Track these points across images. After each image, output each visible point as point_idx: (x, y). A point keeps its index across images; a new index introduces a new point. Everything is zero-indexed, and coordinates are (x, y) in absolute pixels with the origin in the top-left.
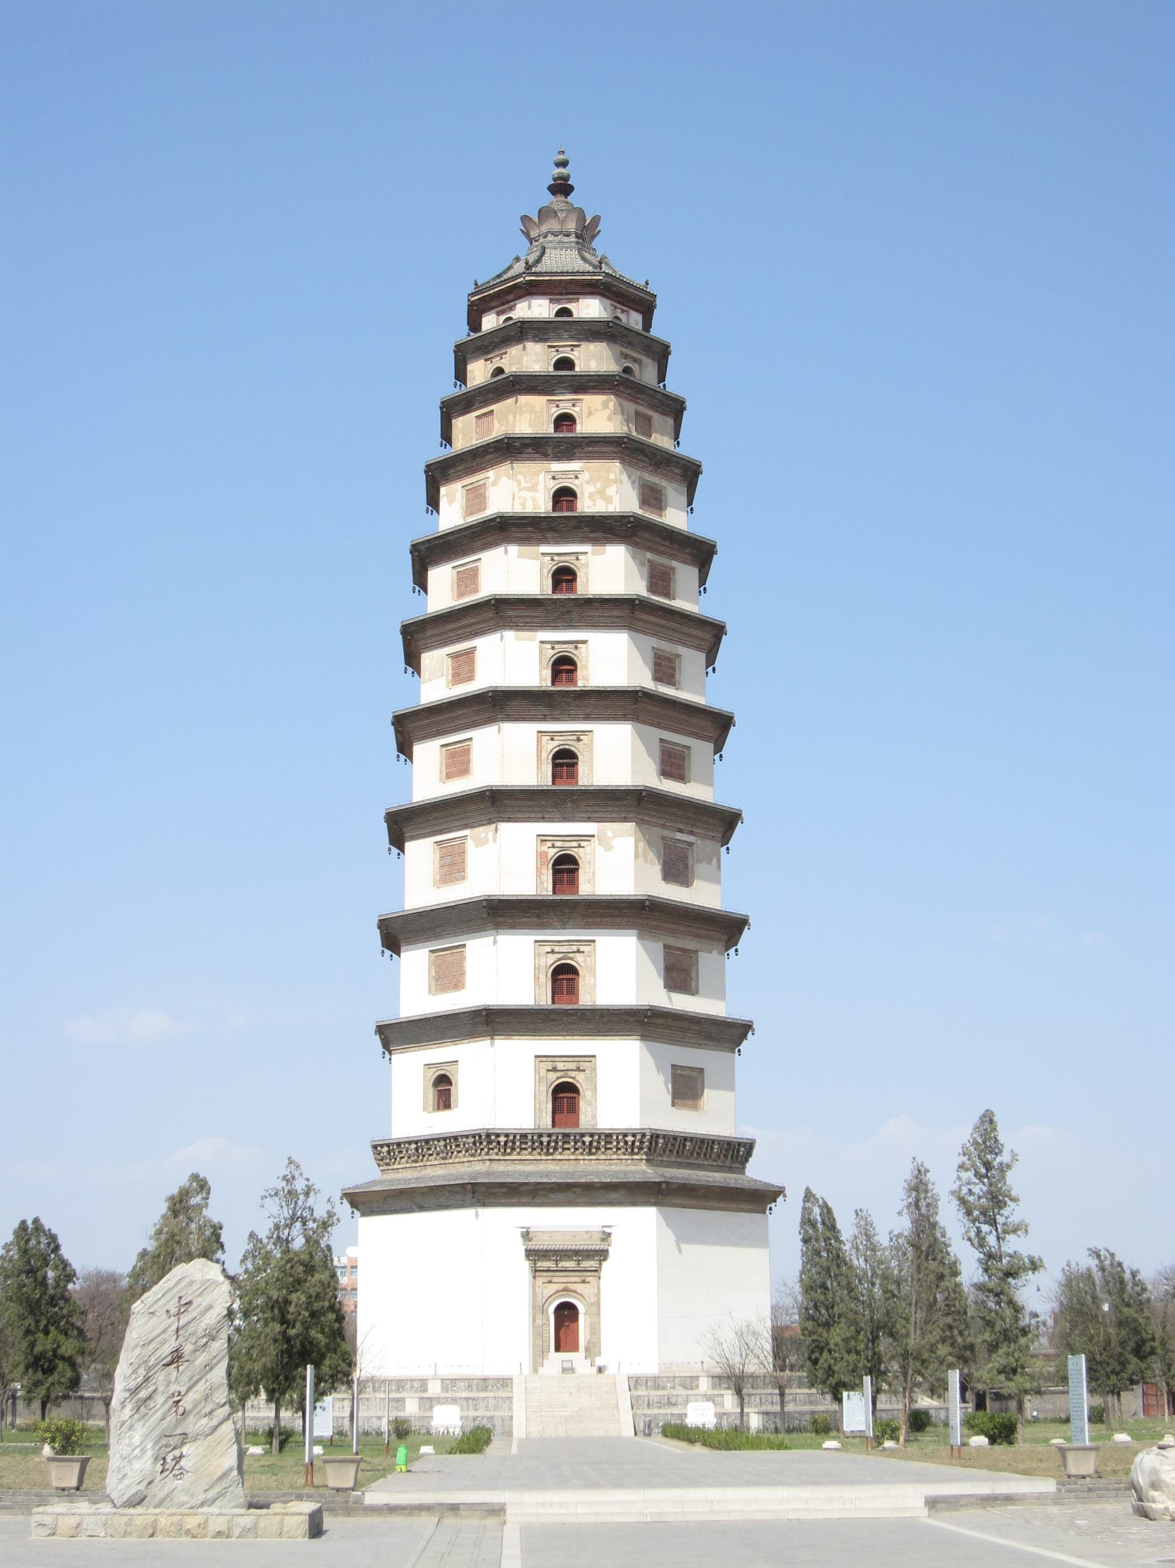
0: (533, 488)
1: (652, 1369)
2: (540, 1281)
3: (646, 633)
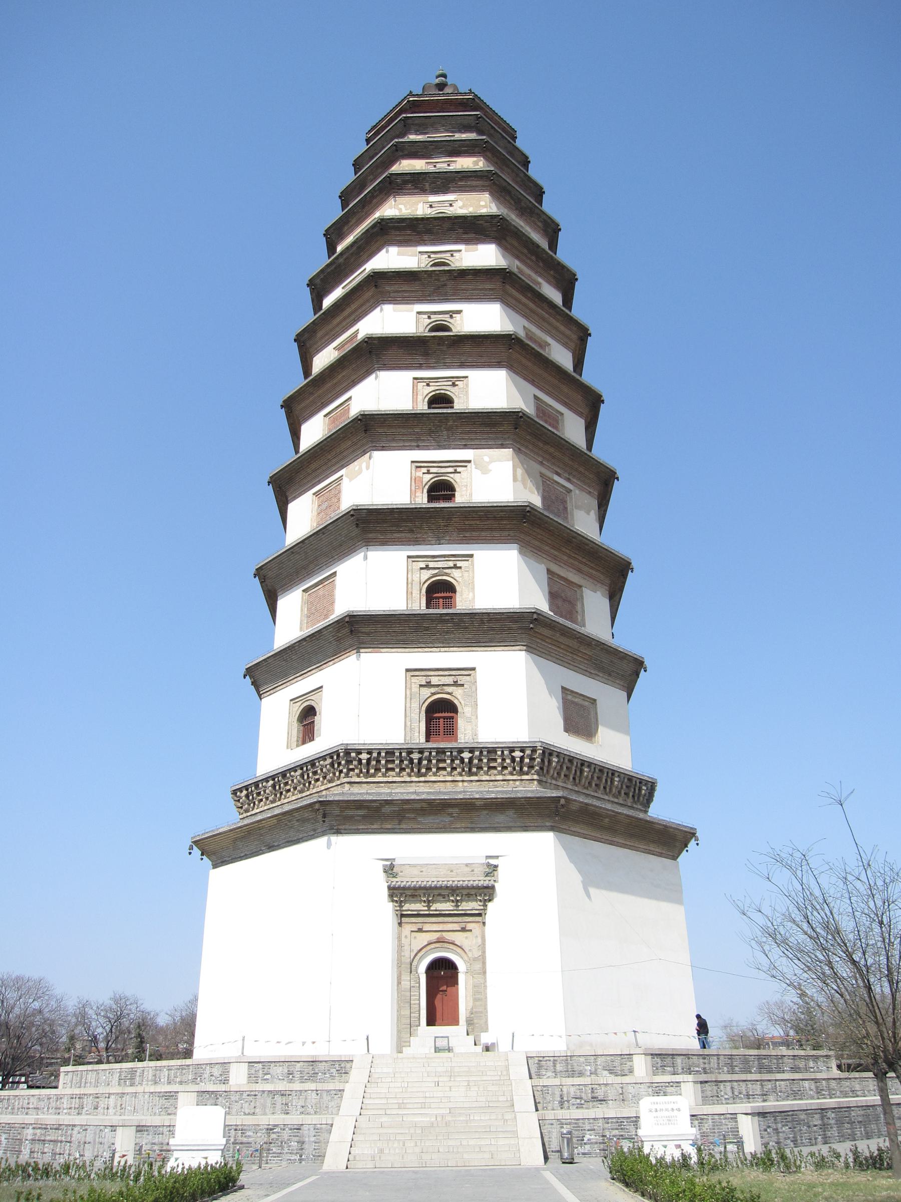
1: (557, 1046)
2: (407, 928)
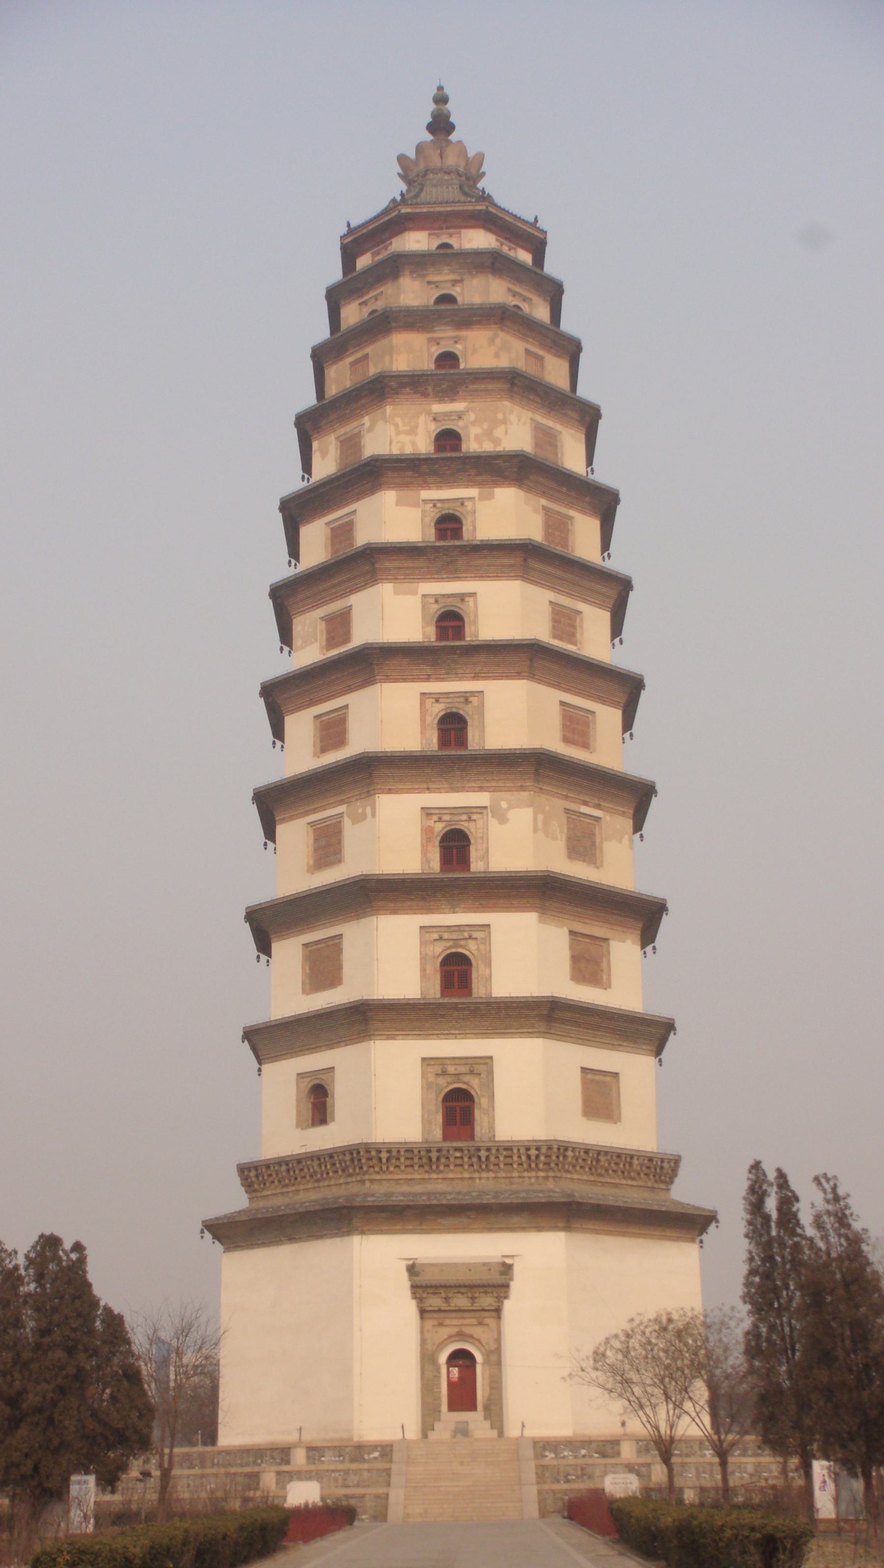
0: (413, 431)
2: (429, 1323)
3: (542, 586)
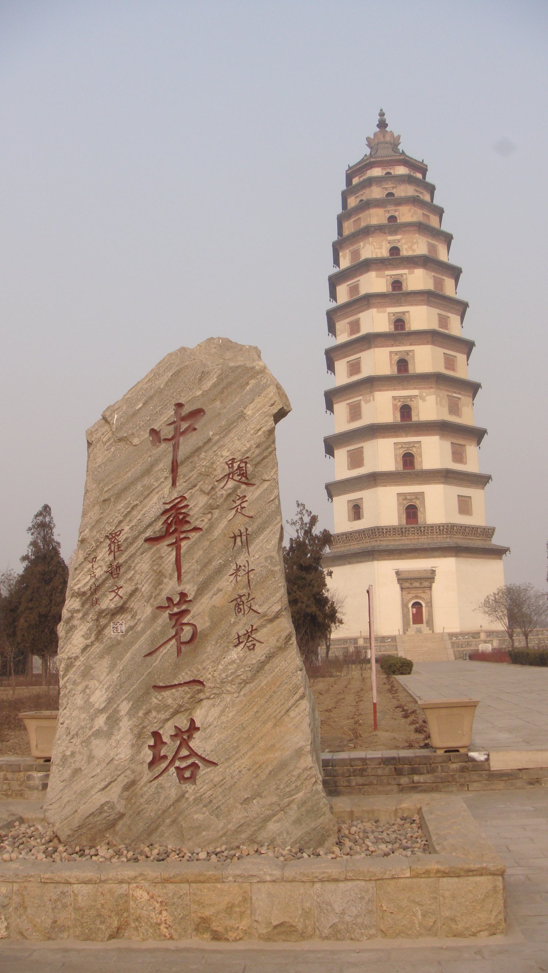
0: (381, 248)
2: (405, 593)
